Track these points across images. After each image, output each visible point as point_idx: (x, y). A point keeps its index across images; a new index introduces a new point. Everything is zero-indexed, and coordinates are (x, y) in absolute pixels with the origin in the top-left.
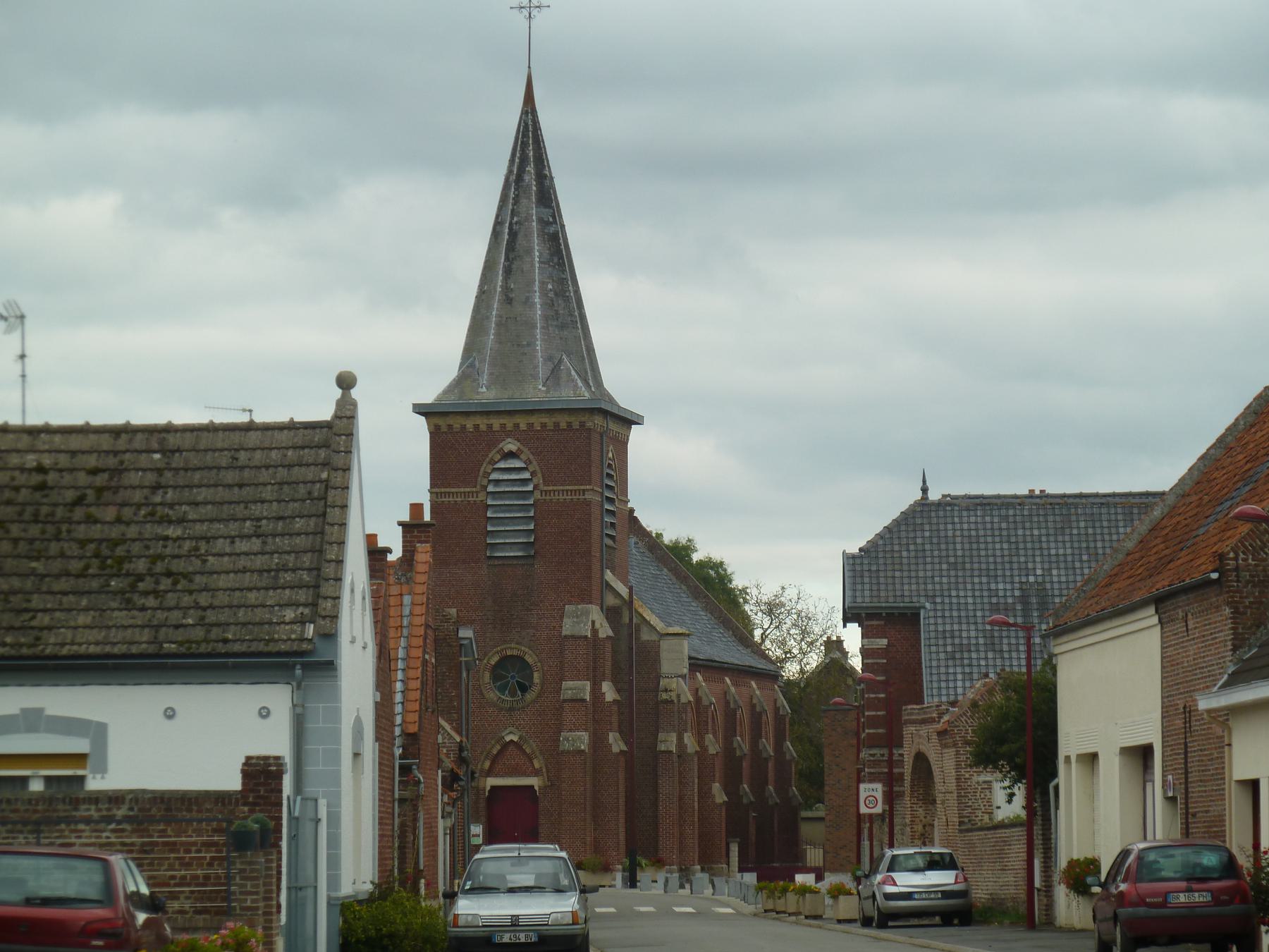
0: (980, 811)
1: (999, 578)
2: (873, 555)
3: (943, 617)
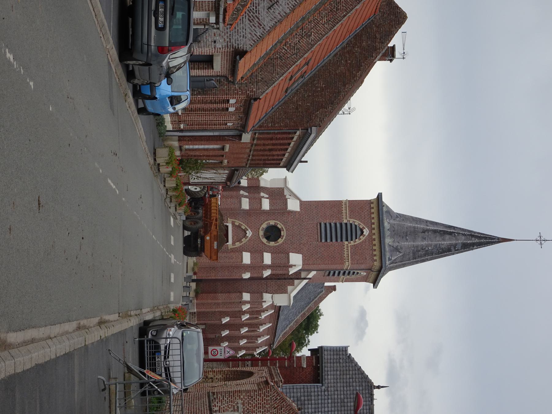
0: (220, 405)
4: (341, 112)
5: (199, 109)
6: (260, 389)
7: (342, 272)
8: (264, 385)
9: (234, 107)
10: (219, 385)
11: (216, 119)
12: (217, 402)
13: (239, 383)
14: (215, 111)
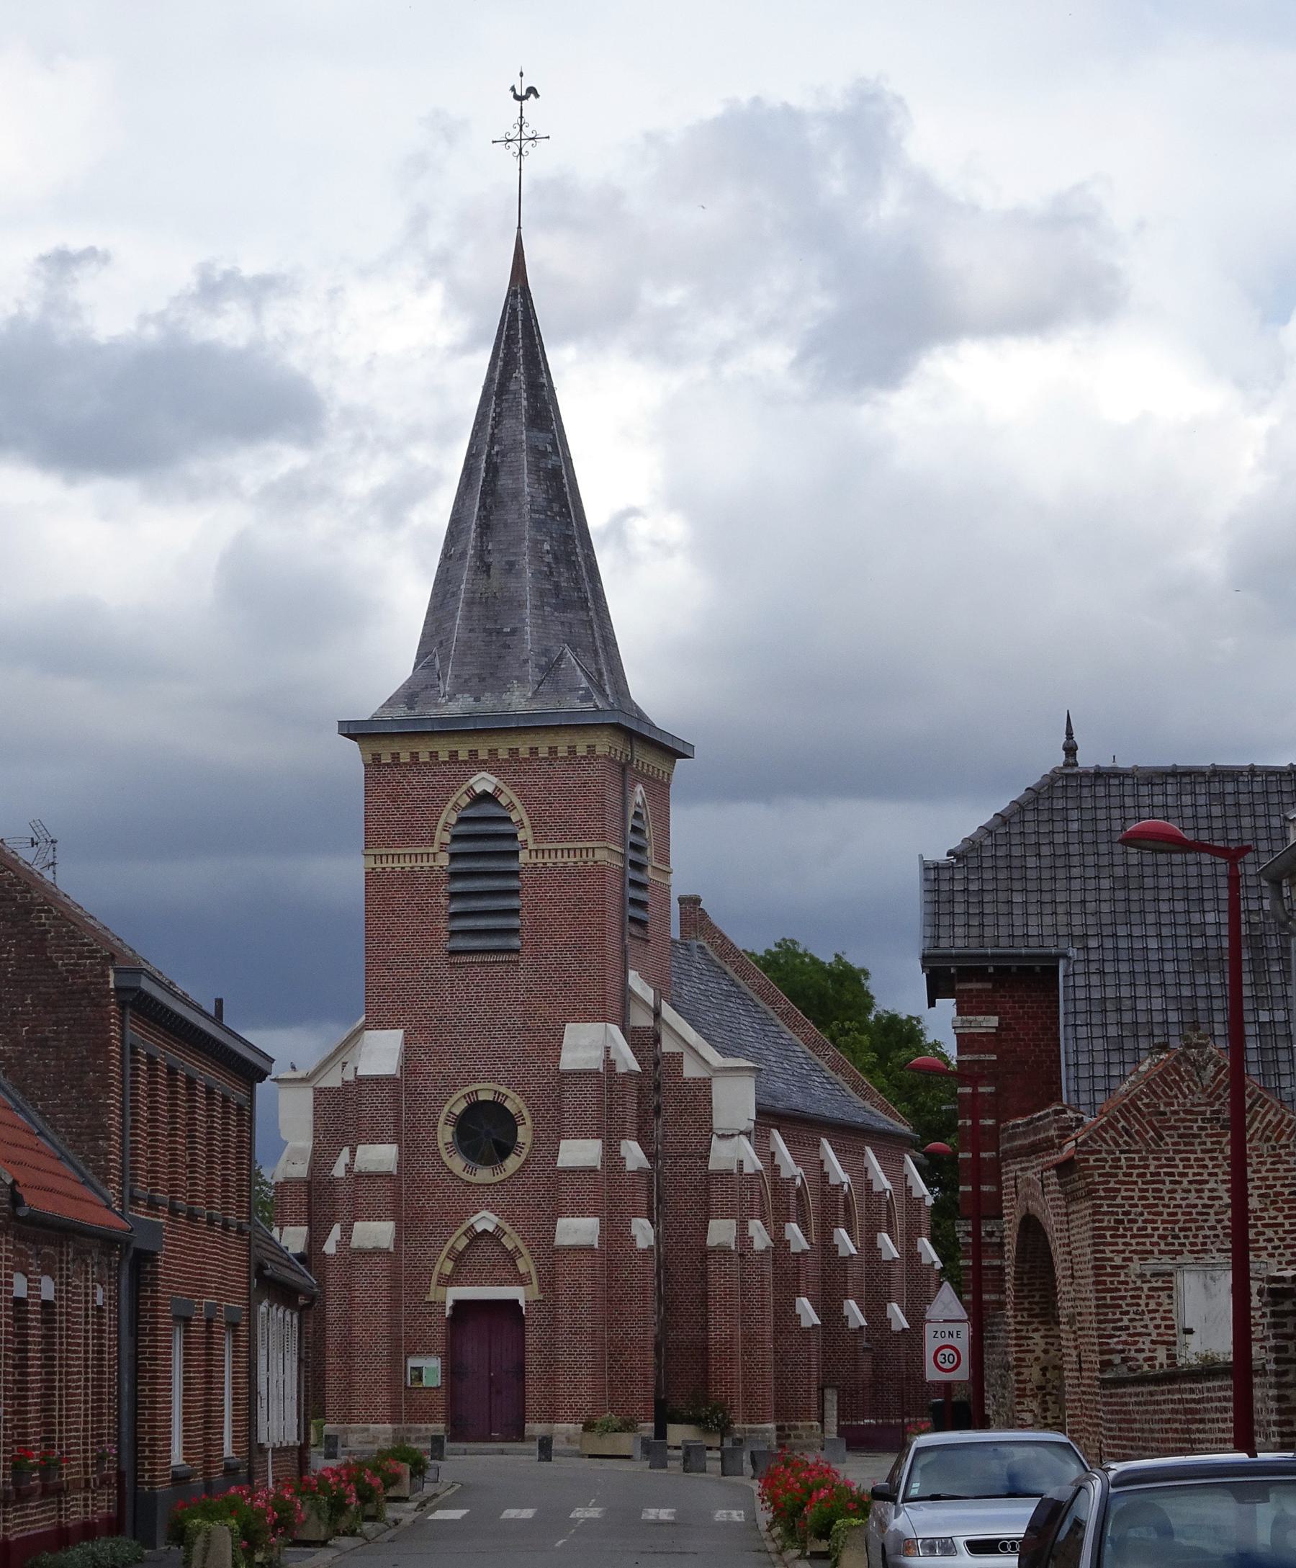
1: (1206, 904)
2: (974, 863)
3: (1102, 973)
4: (48, 875)
5: (46, 1410)
6: (1090, 1194)
7: (632, 874)
8: (1076, 1176)
9: (40, 1281)
10: (1072, 1344)
11: (82, 1348)
12: (1138, 1351)
13: (1065, 1269)
14: (54, 1351)
